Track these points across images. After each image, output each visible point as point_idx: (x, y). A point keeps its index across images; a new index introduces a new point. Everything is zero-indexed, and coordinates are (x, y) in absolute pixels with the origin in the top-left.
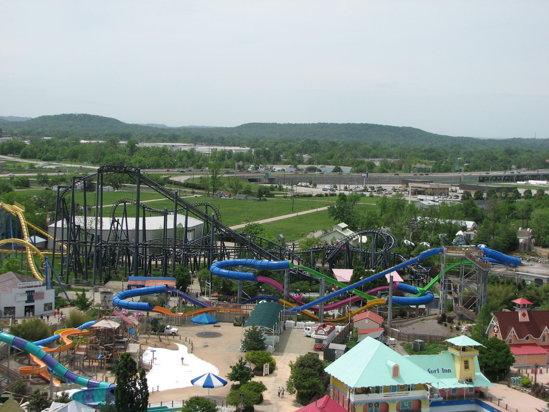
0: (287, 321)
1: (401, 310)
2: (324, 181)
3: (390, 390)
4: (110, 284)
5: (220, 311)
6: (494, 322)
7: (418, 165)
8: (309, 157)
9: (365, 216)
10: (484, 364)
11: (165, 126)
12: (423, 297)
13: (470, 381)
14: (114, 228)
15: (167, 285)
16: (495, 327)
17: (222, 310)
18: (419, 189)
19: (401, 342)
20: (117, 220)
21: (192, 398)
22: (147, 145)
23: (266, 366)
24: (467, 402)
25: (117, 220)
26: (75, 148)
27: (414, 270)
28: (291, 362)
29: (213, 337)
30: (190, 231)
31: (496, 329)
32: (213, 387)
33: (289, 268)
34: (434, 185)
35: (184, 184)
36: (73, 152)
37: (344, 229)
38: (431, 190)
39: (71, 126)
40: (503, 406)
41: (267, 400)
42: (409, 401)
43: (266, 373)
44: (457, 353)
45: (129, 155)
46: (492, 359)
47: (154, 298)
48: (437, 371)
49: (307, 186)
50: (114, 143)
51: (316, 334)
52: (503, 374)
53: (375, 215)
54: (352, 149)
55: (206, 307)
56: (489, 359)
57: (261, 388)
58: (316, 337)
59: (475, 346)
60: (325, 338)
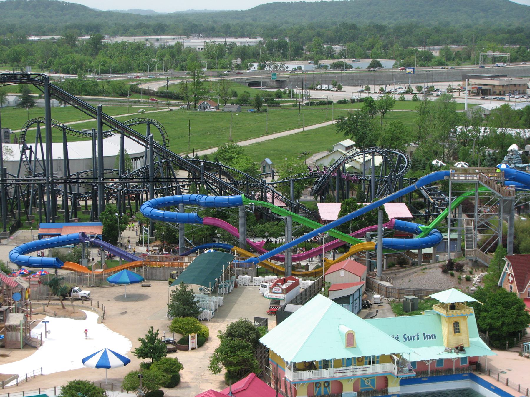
0: (241, 276)
1: (399, 257)
2: (351, 81)
3: (343, 364)
4: (19, 233)
5: (152, 266)
6: (508, 269)
7: (490, 53)
8: (343, 48)
9: (388, 127)
10: (488, 327)
11: (154, 11)
12: (427, 238)
13: (461, 349)
14: (26, 158)
15: (83, 233)
16: (509, 275)
17: (154, 264)
18: (484, 87)
19: (390, 299)
20: (29, 147)
21: (71, 383)
22: (119, 39)
23: (192, 337)
24: (458, 377)
25: (29, 147)
26: (18, 48)
27: (432, 201)
28: (220, 332)
29: (137, 301)
30: (139, 158)
31: (511, 278)
32: (108, 367)
33: (242, 204)
34: (504, 81)
35: (157, 92)
36: (14, 54)
37: (348, 148)
38: (501, 88)
39: (21, 17)
40: (503, 381)
41: (186, 382)
42: (371, 378)
43: (193, 347)
44: (443, 312)
45: (92, 55)
46: (498, 318)
47: (67, 250)
48: (416, 338)
49: (329, 90)
50: (70, 40)
51: (271, 292)
52: (515, 339)
53: (400, 127)
54: (406, 34)
55: (135, 261)
56: (494, 319)
57: (177, 366)
58: (270, 297)
59: (467, 302)
60: (281, 298)
